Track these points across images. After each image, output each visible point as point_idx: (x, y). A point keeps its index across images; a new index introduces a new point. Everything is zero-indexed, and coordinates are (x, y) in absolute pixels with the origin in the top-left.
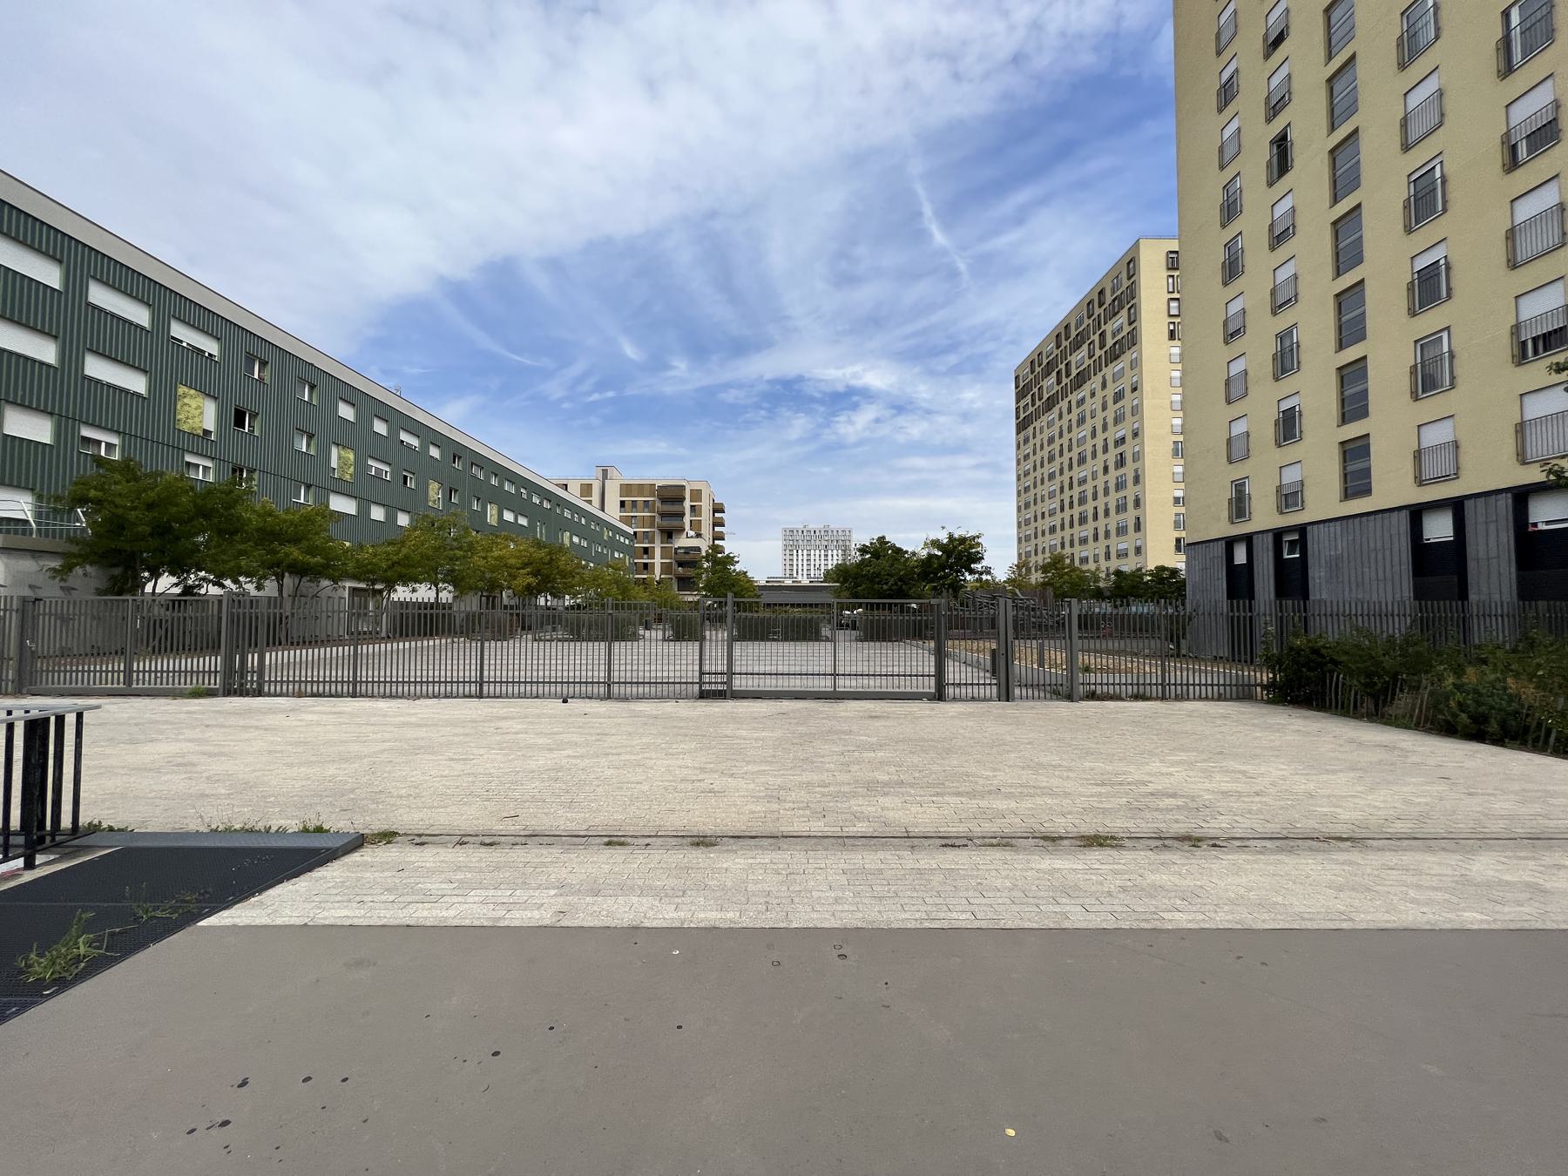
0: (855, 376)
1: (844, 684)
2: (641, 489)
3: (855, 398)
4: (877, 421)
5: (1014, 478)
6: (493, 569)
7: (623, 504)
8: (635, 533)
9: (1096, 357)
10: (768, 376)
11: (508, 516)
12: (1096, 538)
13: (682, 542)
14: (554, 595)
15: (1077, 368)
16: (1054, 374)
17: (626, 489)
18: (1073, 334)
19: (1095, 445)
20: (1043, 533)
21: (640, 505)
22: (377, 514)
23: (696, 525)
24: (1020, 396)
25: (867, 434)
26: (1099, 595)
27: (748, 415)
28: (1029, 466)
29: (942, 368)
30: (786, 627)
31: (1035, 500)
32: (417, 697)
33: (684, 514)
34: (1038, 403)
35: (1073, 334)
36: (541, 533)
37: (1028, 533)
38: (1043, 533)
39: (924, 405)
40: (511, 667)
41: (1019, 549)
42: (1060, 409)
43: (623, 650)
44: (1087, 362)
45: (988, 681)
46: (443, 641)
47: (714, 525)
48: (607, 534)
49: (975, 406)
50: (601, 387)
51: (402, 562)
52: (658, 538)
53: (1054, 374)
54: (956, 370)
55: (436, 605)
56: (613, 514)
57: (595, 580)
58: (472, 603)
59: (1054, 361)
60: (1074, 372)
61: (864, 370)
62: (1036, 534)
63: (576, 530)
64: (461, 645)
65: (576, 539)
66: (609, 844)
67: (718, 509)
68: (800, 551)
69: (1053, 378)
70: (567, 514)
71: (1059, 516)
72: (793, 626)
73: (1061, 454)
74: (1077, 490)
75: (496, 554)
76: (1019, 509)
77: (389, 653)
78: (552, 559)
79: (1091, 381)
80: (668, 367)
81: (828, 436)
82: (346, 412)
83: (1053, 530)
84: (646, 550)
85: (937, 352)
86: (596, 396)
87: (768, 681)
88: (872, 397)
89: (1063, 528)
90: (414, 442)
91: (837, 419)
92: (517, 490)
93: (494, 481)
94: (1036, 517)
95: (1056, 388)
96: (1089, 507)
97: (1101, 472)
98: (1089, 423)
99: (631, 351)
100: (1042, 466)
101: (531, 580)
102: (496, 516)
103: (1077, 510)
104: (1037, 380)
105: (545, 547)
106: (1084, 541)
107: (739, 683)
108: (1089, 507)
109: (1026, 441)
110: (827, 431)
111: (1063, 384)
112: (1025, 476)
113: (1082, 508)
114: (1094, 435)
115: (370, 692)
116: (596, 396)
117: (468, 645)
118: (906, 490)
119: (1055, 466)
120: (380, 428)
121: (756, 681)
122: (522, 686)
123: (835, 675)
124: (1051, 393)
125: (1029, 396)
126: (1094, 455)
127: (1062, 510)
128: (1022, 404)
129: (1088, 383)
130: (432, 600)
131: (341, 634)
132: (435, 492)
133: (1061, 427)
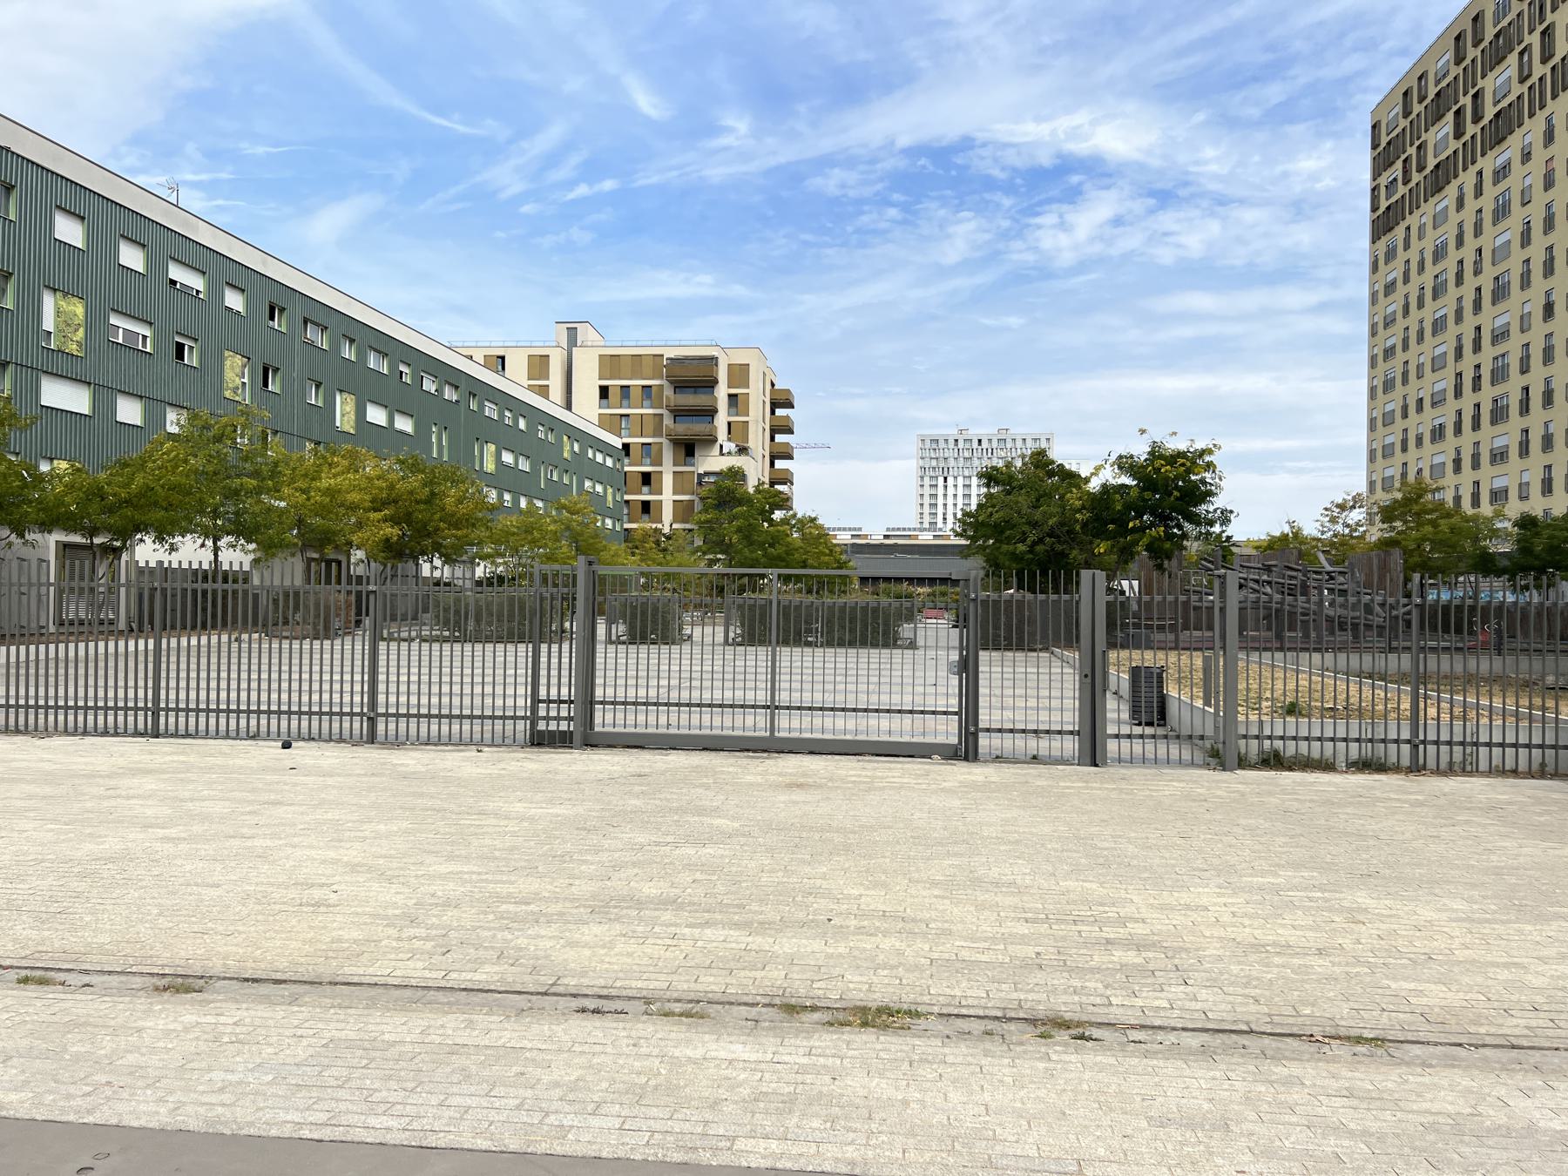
0: (1074, 133)
1: (789, 726)
2: (636, 363)
3: (1075, 179)
4: (1117, 221)
5: (1365, 329)
6: (322, 511)
7: (604, 392)
8: (626, 447)
9: (1535, 79)
10: (904, 141)
11: (376, 415)
12: (1524, 450)
13: (712, 462)
14: (448, 560)
15: (1496, 103)
16: (1450, 116)
17: (611, 364)
18: (1490, 32)
19: (1528, 261)
20: (1419, 441)
21: (636, 394)
22: (129, 411)
23: (737, 432)
24: (1381, 163)
25: (1097, 248)
26: (1486, 565)
27: (865, 219)
28: (1396, 306)
29: (1254, 112)
30: (830, 622)
31: (1405, 375)
32: (46, 733)
33: (715, 411)
34: (1416, 177)
35: (1490, 32)
36: (439, 445)
37: (1388, 440)
38: (1419, 441)
39: (1213, 186)
40: (275, 686)
41: (1370, 472)
42: (1460, 188)
43: (510, 659)
44: (1517, 89)
45: (1125, 730)
46: (214, 639)
47: (773, 432)
48: (569, 449)
49: (1318, 186)
50: (592, 170)
51: (135, 500)
52: (668, 455)
53: (1450, 116)
54: (1282, 115)
55: (216, 574)
56: (587, 412)
57: (530, 530)
58: (289, 572)
59: (1451, 91)
60: (1489, 112)
61: (1095, 123)
62: (1404, 443)
63: (507, 439)
64: (255, 646)
65: (508, 458)
66: (25, 981)
67: (781, 401)
68: (950, 481)
69: (1447, 125)
70: (490, 410)
71: (1452, 405)
72: (842, 618)
73: (1459, 280)
74: (1489, 351)
75: (325, 483)
76: (1372, 391)
77: (101, 657)
78: (433, 494)
79: (1524, 129)
80: (715, 130)
81: (1019, 254)
82: (69, 231)
83: (1438, 433)
84: (646, 478)
85: (1242, 79)
86: (582, 190)
87: (750, 720)
88: (1110, 175)
89: (1458, 430)
90: (195, 282)
91: (1038, 220)
92: (392, 367)
93: (348, 352)
94: (1405, 408)
95: (1454, 145)
96: (1512, 388)
97: (1538, 313)
98: (1517, 215)
99: (646, 102)
100: (1421, 305)
101: (392, 531)
102: (353, 416)
103: (1488, 393)
104: (1415, 130)
105: (423, 472)
106: (1499, 456)
107: (604, 720)
108: (1512, 388)
109: (1390, 255)
110: (1018, 244)
111: (1467, 137)
112: (1386, 326)
113: (1498, 390)
114: (1526, 239)
115: (172, 727)
116: (582, 190)
117: (265, 646)
118: (1172, 358)
119: (1447, 306)
120: (131, 257)
121: (706, 718)
122: (315, 719)
123: (773, 707)
124: (1443, 157)
125: (1399, 164)
126: (1526, 282)
127: (1458, 393)
128: (1384, 180)
129: (1518, 133)
130: (205, 566)
131: (43, 623)
132: (235, 372)
133: (1460, 225)
